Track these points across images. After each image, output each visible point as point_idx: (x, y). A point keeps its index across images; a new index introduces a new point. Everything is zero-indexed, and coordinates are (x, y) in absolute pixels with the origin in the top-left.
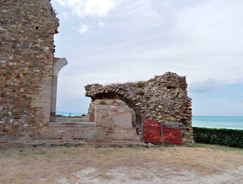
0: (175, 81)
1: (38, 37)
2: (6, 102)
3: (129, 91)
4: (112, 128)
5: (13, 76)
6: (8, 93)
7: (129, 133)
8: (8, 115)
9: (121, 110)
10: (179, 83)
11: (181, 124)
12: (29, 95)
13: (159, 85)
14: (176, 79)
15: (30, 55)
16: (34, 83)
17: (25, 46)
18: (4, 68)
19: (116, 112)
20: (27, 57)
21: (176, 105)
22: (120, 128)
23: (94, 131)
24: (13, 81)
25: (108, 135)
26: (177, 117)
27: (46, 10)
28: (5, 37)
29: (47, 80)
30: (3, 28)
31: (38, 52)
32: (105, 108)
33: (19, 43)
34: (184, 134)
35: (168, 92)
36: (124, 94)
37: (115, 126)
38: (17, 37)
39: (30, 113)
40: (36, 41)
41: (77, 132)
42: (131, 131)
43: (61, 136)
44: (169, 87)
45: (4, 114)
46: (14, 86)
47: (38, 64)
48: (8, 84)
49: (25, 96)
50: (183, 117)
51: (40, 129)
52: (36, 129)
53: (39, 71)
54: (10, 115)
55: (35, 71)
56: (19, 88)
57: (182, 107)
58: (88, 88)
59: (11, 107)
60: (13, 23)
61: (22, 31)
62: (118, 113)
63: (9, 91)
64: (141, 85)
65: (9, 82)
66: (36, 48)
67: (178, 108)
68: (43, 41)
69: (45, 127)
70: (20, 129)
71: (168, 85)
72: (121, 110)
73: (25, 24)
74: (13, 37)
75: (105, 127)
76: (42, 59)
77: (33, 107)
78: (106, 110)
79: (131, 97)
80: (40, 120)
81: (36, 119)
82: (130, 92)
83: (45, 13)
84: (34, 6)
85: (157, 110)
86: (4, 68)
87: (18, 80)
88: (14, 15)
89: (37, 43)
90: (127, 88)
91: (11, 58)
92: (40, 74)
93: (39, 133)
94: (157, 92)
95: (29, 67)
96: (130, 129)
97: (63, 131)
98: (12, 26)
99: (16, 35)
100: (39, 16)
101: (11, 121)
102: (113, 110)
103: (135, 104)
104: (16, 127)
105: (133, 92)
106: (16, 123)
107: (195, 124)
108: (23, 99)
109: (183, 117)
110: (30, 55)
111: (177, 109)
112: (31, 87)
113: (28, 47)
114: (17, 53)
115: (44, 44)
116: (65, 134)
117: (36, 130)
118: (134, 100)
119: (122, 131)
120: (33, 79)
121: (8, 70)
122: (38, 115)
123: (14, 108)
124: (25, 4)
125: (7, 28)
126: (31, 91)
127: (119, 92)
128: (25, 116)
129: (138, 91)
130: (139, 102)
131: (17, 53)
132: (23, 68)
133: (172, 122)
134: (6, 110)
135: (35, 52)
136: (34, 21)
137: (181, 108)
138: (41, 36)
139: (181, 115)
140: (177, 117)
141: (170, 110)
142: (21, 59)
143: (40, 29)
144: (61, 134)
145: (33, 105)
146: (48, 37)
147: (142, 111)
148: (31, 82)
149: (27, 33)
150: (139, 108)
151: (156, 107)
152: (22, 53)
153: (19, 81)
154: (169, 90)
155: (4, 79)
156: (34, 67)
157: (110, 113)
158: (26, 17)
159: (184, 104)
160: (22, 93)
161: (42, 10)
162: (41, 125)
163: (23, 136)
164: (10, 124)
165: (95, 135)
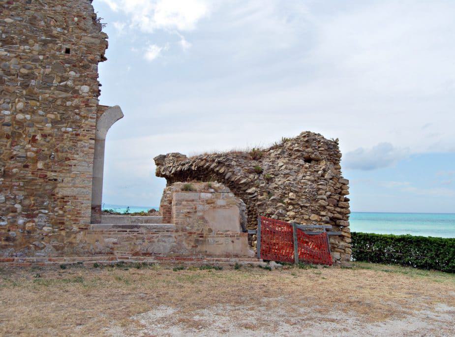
0: (319, 147)
4: (205, 233)
6: (15, 170)
8: (14, 211)
9: (220, 202)
11: (329, 226)
12: (53, 174)
13: (290, 155)
14: (320, 145)
16: (62, 152)
17: (46, 84)
18: (8, 125)
19: (212, 205)
20: (50, 105)
21: (319, 192)
22: (220, 234)
23: (171, 240)
25: (196, 246)
26: (323, 213)
27: (84, 18)
30: (6, 51)
31: (70, 95)
33: (35, 78)
35: (306, 168)
36: (226, 171)
37: (210, 231)
38: (31, 69)
39: (54, 207)
40: (66, 75)
42: (238, 239)
44: (308, 160)
45: (8, 209)
46: (26, 157)
48: (15, 153)
49: (46, 176)
50: (334, 213)
51: (73, 236)
53: (70, 129)
54: (19, 210)
55: (63, 129)
56: (35, 161)
57: (331, 195)
59: (21, 195)
60: (25, 42)
61: (41, 57)
64: (257, 155)
65: (17, 151)
66: (66, 89)
67: (325, 197)
68: (78, 75)
69: (82, 232)
70: (38, 236)
71: (306, 155)
72: (220, 202)
73: (45, 43)
74: (24, 67)
75: (191, 233)
76: (77, 107)
77: (60, 195)
78: (193, 201)
80: (73, 220)
81: (65, 218)
83: (81, 24)
86: (8, 125)
89: (67, 79)
91: (20, 105)
93: (71, 243)
94: (286, 168)
95: (54, 122)
97: (115, 240)
98: (22, 48)
99: (30, 64)
100: (70, 30)
101: (21, 221)
102: (207, 200)
103: (247, 190)
104: (29, 232)
107: (355, 226)
108: (42, 180)
109: (334, 213)
110: (55, 100)
111: (322, 199)
114: (31, 96)
115: (80, 81)
116: (119, 246)
117: (66, 238)
119: (222, 240)
120: (61, 145)
123: (26, 197)
124: (46, 7)
125: (13, 52)
126: (56, 167)
127: (217, 169)
128: (47, 211)
130: (253, 186)
132: (43, 124)
133: (314, 222)
135: (64, 95)
136: (62, 39)
137: (329, 197)
138: (75, 66)
140: (323, 213)
142: (38, 108)
143: (72, 52)
144: (111, 245)
145: (61, 192)
146: (88, 68)
147: (259, 203)
148: (57, 151)
152: (40, 98)
153: (34, 149)
156: (63, 123)
157: (200, 208)
158: (47, 32)
159: (335, 190)
160: (41, 170)
161: (76, 19)
162: (75, 228)
164: (18, 227)
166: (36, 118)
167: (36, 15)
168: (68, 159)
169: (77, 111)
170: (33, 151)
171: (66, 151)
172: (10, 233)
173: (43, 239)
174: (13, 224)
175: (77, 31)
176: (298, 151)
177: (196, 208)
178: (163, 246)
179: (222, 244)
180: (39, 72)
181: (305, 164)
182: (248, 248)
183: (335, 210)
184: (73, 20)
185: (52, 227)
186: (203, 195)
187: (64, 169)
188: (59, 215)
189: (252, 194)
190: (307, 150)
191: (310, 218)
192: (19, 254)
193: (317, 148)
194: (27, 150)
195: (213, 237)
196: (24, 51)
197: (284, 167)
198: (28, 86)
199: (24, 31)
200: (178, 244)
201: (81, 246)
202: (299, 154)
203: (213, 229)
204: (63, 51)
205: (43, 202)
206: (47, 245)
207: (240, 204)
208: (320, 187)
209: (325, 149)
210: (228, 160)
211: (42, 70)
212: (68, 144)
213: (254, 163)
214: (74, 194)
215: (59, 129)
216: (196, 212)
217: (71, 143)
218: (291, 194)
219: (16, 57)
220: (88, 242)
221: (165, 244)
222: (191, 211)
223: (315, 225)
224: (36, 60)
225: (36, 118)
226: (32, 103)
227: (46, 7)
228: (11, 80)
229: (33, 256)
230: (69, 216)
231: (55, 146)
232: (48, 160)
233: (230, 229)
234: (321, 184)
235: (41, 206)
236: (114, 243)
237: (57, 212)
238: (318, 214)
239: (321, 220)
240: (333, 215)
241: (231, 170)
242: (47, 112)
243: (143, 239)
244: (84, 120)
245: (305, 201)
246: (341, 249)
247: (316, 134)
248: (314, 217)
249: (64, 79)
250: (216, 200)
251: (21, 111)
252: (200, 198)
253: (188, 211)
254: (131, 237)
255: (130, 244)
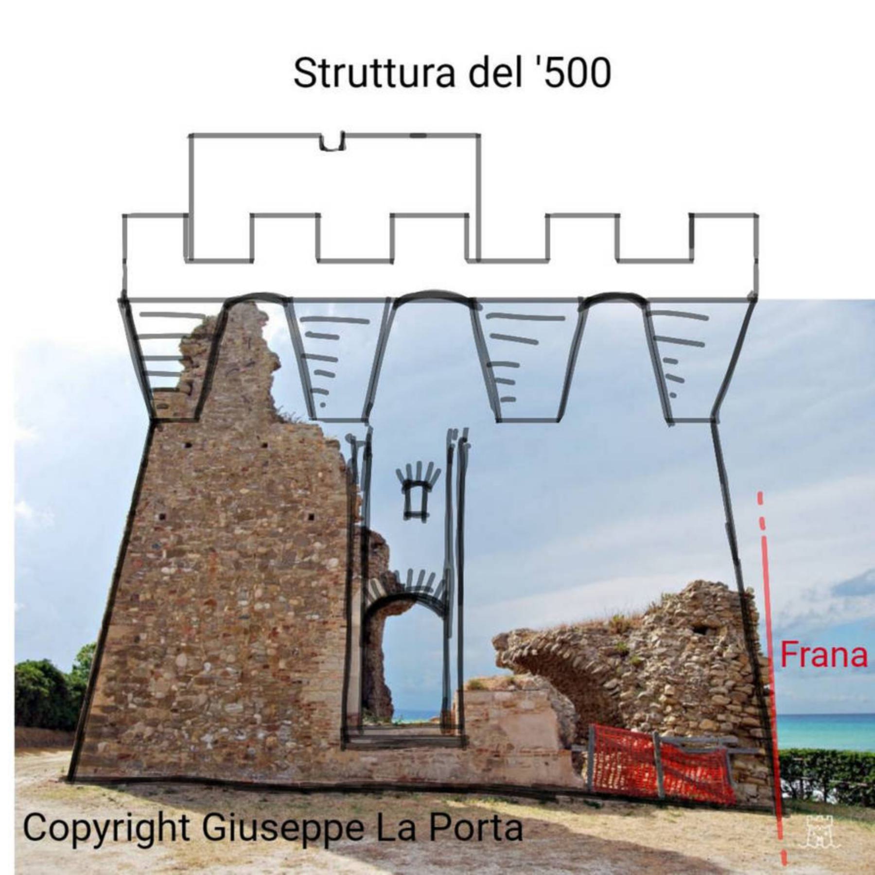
0: (716, 606)
1: (314, 537)
2: (250, 694)
3: (587, 647)
4: (502, 750)
5: (263, 633)
6: (253, 673)
7: (550, 767)
8: (254, 722)
9: (525, 704)
10: (728, 614)
11: (733, 739)
12: (297, 675)
13: (671, 622)
14: (716, 603)
15: (297, 582)
16: (308, 646)
17: (288, 560)
18: (246, 617)
19: (513, 709)
20: (293, 589)
21: (714, 681)
22: (525, 752)
23: (453, 760)
24: (263, 643)
25: (489, 770)
26: (721, 717)
27: (330, 472)
28: (246, 547)
29: (334, 637)
30: (242, 528)
31: (315, 572)
32: (481, 699)
33: (274, 556)
34: (748, 773)
35: (694, 643)
36: (574, 655)
37: (511, 747)
38: (270, 545)
39: (299, 717)
40: (309, 548)
41: (407, 762)
42: (555, 760)
43: (371, 771)
44: (700, 629)
45: (246, 720)
46: (267, 656)
47: (315, 601)
48: (253, 651)
49: (288, 677)
50: (742, 717)
51: (321, 753)
52: (313, 753)
53: (316, 617)
54: (258, 722)
55: (308, 617)
56: (276, 659)
57: (734, 686)
58: (501, 643)
59: (260, 703)
60: (262, 514)
61: (281, 530)
62: (516, 713)
63: (255, 669)
64: (622, 628)
65: (256, 648)
66: (310, 565)
67: (723, 689)
68: (324, 546)
69: (332, 750)
70: (279, 753)
71: (695, 621)
72: (525, 704)
73: (285, 511)
74: (262, 544)
75: (481, 751)
76: (325, 587)
77: (305, 702)
78: (483, 703)
79: (591, 664)
80: (321, 733)
81: (312, 731)
82: (589, 650)
83: (328, 480)
84: (303, 467)
85: (663, 698)
86: (246, 617)
87: (273, 641)
88: (262, 496)
89: (311, 553)
90: (580, 639)
91: (259, 593)
92: (319, 623)
93: (319, 763)
94: (661, 645)
95: (298, 610)
96: (554, 755)
97: (374, 760)
98: (259, 522)
99: (269, 540)
100: (314, 490)
101: (261, 735)
102: (504, 702)
103: (604, 683)
104: (270, 749)
105: (597, 648)
106: (270, 740)
107: (787, 740)
108: (284, 683)
109: (742, 717)
110: (297, 582)
111: (718, 693)
112: (300, 656)
113: (292, 565)
114: (271, 580)
115: (326, 553)
116: (379, 767)
117: (312, 756)
118: (602, 674)
119: (529, 761)
120: (306, 637)
121: (252, 620)
122: (317, 721)
123: (266, 706)
124: (285, 467)
125: (249, 529)
126: (301, 666)
127: (560, 652)
128: (290, 722)
129: (611, 644)
130: (614, 676)
131: (271, 580)
132: (285, 612)
133: (706, 733)
134: (251, 711)
135: (308, 573)
136: (304, 503)
137: (733, 688)
138: (320, 535)
139: (732, 712)
140: (721, 717)
141: (697, 697)
142: (279, 594)
143: (317, 518)
144: (369, 767)
145: (306, 698)
146: (336, 535)
147: (622, 703)
148: (301, 645)
149: (289, 532)
150: (614, 694)
151: (658, 691)
152: (281, 581)
153: (276, 645)
154: (695, 638)
155: (246, 641)
156: (308, 609)
157: (493, 713)
158: (287, 497)
159: (744, 676)
160: (283, 670)
161: (320, 474)
162: (324, 743)
163: (285, 769)
164: (257, 741)
165: (455, 770)
166: (277, 606)
167: (274, 478)
168: (314, 654)
169: (324, 592)
170: (274, 648)
171: (313, 645)
172: (250, 749)
173: (286, 757)
174: (253, 738)
175: (322, 489)
176: (681, 615)
177: (487, 715)
178: (440, 768)
179: (529, 767)
180: (280, 547)
181: (693, 635)
182: (573, 773)
183: (743, 711)
184: (317, 476)
185: (297, 742)
186: (498, 695)
187: (310, 668)
188: (305, 727)
189: (612, 689)
190: (695, 612)
191: (701, 726)
192: (259, 775)
193: (712, 607)
194: (266, 648)
195: (515, 756)
196: (261, 526)
197: (659, 642)
198: (266, 567)
199: (261, 500)
200: (463, 766)
201: (332, 766)
202: (682, 620)
203: (515, 744)
204: (306, 518)
205: (286, 711)
206: (291, 764)
207: (563, 706)
208: (713, 672)
209: (726, 609)
210: (575, 637)
211: (282, 546)
212: (314, 635)
213: (617, 639)
214: (321, 699)
215: (303, 617)
216: (487, 720)
217: (318, 634)
218: (667, 687)
219: (253, 534)
220: (340, 761)
221: (442, 766)
222: (481, 718)
223: (709, 736)
224: (275, 535)
225: (277, 606)
226: (271, 588)
227: (285, 467)
228: (248, 563)
229: (274, 779)
230: (316, 728)
231: (298, 640)
232: (290, 658)
233: (541, 744)
234: (716, 669)
235: (284, 716)
236: (374, 764)
237: (302, 723)
238: (714, 719)
239: (718, 730)
240: (740, 720)
241: (580, 652)
242: (288, 596)
243: (412, 758)
244: (332, 604)
245: (689, 696)
246: (758, 778)
247: (712, 584)
248: (706, 724)
249: (307, 553)
250: (518, 701)
251: (261, 600)
252: (493, 699)
253: (477, 718)
254: (782, 786)
255: (395, 765)
